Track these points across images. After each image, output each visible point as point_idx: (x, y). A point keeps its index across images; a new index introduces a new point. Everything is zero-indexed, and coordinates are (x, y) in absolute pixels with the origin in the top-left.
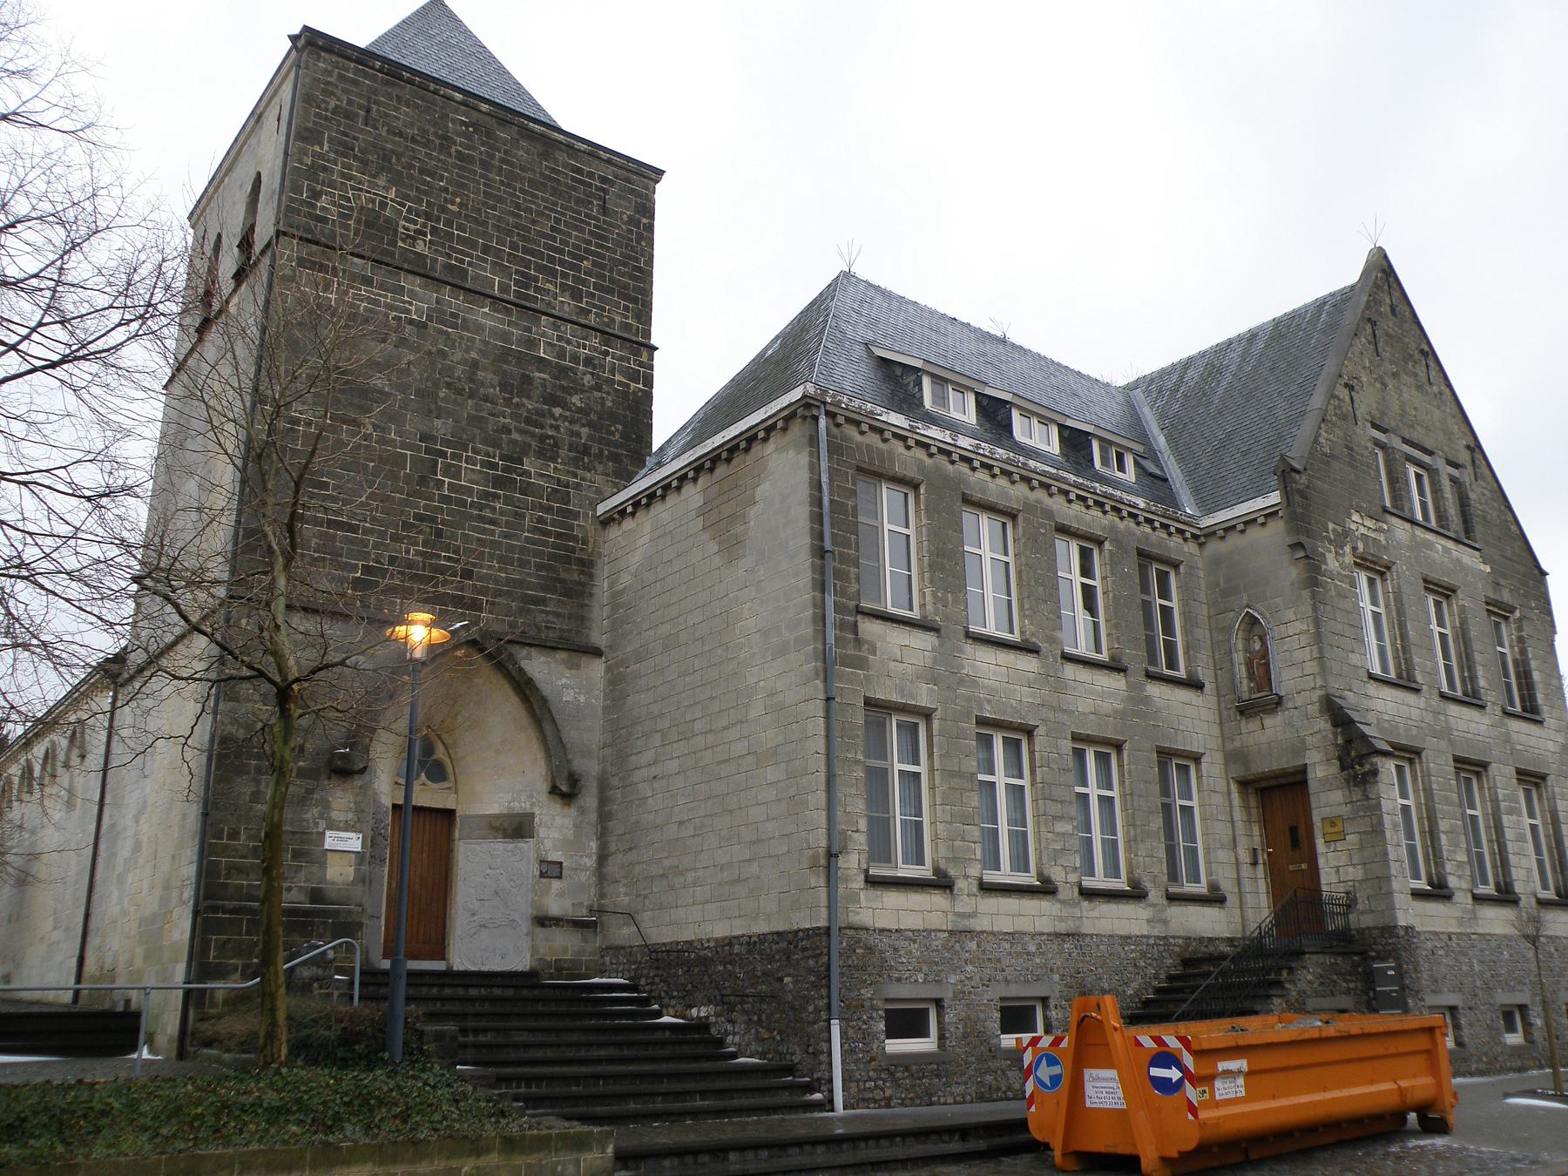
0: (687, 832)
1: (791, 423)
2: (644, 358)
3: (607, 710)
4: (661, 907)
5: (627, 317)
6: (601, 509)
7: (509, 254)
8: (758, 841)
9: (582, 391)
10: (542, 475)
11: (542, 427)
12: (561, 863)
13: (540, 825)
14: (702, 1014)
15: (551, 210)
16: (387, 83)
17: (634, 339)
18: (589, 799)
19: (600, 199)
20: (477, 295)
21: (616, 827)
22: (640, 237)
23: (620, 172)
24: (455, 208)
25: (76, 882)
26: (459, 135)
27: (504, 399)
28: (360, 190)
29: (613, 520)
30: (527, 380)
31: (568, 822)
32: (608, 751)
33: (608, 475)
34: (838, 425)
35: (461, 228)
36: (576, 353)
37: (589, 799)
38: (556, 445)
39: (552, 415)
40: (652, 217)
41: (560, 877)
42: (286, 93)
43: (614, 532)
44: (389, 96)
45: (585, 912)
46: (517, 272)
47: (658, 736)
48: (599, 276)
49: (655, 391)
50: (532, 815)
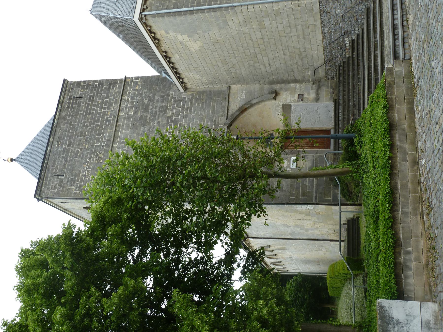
0: (287, 52)
1: (148, 25)
2: (130, 80)
3: (247, 84)
4: (312, 59)
5: (116, 87)
6: (181, 90)
7: (100, 127)
8: (290, 26)
9: (143, 99)
10: (172, 110)
11: (156, 112)
12: (298, 95)
13: (286, 102)
14: (348, 42)
15: (83, 115)
16: (49, 170)
17: (123, 84)
18: (277, 87)
19: (77, 100)
20: (115, 136)
21: (286, 77)
22: (88, 85)
23: (67, 94)
24: (87, 146)
25: (308, 245)
26: (62, 147)
27: (148, 124)
28: (85, 176)
29: (185, 86)
30: (141, 118)
31: (285, 93)
32: (261, 82)
33: (170, 89)
34: (147, 8)
35: (93, 143)
36: (130, 103)
37: (277, 87)
38: (162, 107)
39: (152, 109)
40: (80, 82)
41: (303, 95)
42: (56, 201)
43: (189, 85)
44: (52, 170)
45: (314, 86)
46: (105, 124)
47: (256, 65)
48: (103, 97)
49: (140, 76)
50: (283, 105)
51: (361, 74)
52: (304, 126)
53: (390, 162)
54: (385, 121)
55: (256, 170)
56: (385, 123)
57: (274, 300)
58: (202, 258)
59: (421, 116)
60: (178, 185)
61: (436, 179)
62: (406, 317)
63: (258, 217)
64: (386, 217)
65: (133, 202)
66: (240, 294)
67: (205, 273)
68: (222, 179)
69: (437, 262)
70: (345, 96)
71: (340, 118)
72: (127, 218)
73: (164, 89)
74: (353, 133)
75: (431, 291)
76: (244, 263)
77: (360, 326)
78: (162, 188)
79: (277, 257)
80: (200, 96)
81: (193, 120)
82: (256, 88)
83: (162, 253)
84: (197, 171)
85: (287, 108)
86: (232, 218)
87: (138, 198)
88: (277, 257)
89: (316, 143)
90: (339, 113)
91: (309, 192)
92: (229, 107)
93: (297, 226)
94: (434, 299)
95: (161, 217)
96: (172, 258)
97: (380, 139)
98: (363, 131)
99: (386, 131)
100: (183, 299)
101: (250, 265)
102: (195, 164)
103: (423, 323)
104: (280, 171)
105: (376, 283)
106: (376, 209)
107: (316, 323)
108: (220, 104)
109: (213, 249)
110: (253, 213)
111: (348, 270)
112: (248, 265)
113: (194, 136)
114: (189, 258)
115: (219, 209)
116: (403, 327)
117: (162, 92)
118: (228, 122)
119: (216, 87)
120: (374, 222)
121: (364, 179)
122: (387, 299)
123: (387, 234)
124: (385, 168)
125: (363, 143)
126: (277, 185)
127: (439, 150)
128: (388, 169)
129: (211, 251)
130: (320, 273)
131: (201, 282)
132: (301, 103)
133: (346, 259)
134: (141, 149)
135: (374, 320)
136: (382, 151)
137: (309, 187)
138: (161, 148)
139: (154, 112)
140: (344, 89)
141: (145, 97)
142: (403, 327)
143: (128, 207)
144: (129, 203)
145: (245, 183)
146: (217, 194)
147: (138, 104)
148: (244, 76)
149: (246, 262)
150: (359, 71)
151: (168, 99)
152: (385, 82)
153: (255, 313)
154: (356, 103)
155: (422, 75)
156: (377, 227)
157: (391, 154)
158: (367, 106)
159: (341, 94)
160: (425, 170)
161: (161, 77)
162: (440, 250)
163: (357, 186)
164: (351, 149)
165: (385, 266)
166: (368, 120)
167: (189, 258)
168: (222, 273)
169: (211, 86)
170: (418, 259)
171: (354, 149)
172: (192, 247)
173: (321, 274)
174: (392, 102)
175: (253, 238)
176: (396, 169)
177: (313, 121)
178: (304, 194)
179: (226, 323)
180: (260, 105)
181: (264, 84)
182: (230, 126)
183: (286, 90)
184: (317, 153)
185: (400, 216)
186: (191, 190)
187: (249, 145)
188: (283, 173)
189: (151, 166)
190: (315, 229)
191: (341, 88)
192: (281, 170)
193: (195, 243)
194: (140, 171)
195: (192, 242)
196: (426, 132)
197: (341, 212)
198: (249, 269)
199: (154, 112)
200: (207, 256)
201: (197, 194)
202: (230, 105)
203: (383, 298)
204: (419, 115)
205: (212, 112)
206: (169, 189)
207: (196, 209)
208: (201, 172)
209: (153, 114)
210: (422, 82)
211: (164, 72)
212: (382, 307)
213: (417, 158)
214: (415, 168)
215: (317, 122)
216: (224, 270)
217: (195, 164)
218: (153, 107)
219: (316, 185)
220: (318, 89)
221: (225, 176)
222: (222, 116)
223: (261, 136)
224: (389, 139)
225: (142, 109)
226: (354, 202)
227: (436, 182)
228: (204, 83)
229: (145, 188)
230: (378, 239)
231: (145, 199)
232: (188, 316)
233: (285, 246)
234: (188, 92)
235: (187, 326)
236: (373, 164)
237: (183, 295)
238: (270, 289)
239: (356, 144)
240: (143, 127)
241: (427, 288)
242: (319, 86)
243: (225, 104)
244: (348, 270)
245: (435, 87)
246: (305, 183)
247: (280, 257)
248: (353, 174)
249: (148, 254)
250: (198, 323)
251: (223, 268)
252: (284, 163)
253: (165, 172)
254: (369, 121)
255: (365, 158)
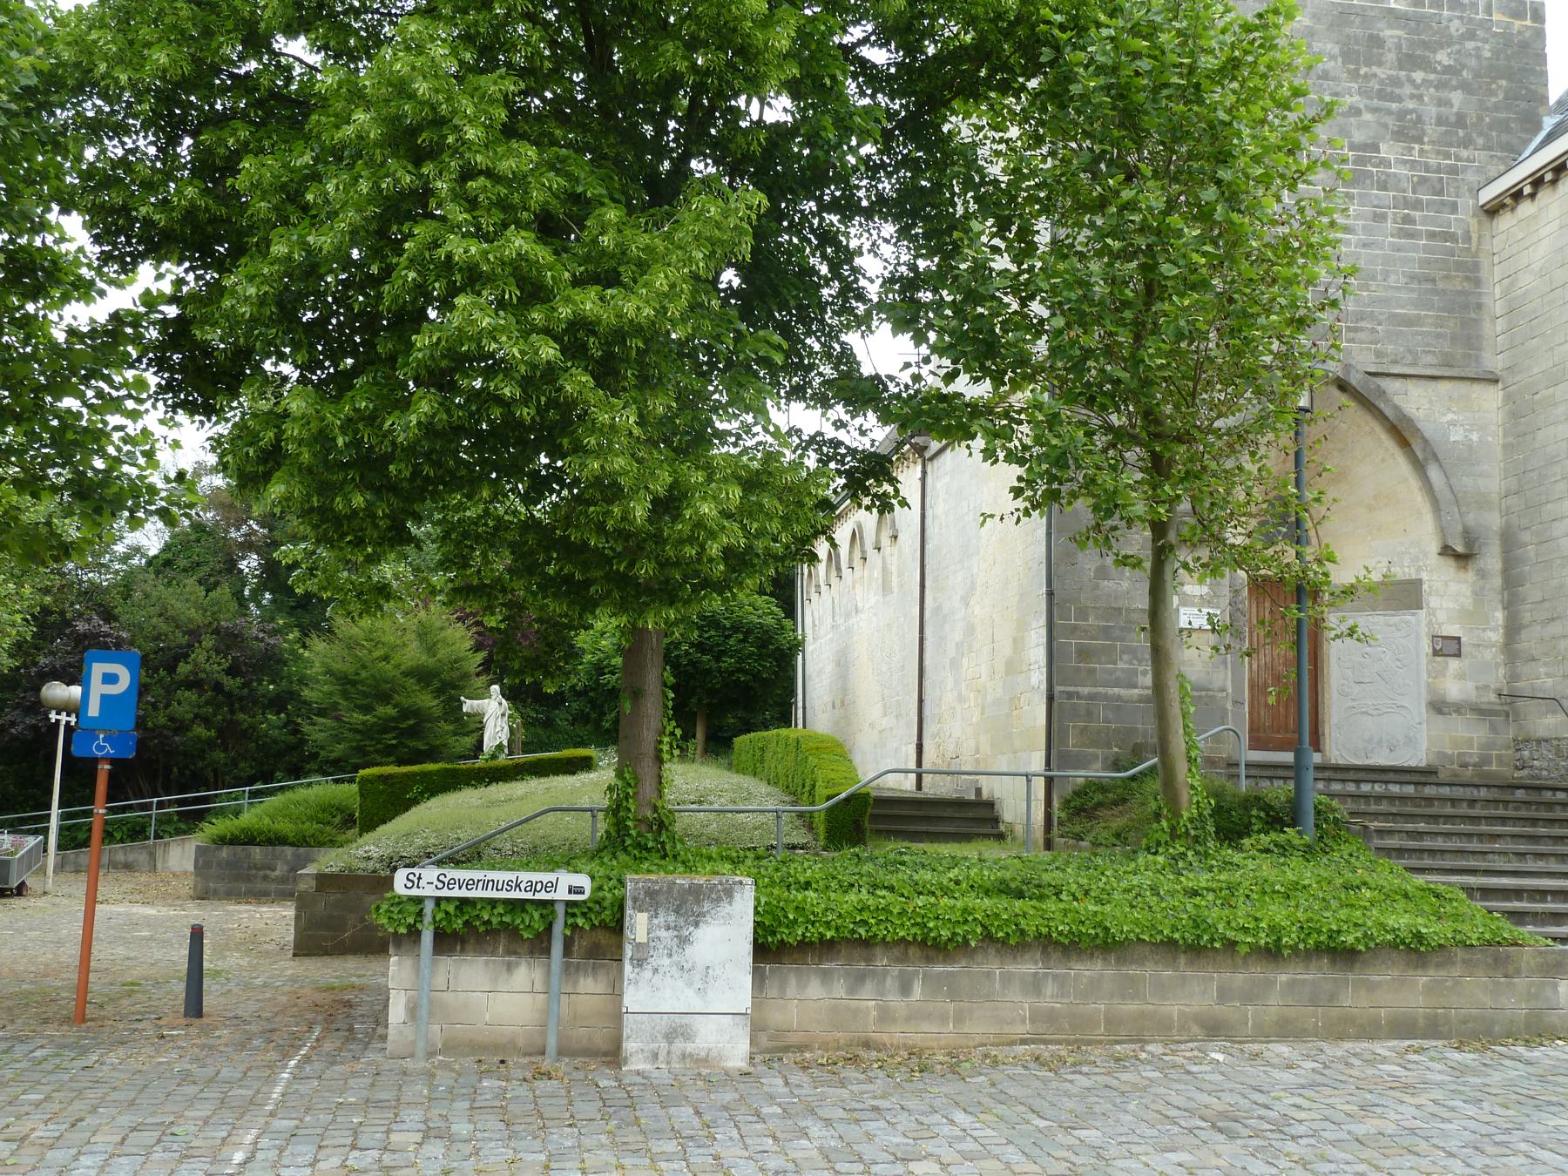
6: (1487, 195)
9: (1449, 46)
10: (1405, 162)
11: (1399, 99)
12: (1458, 639)
18: (1492, 560)
21: (1531, 592)
27: (1349, 72)
29: (1503, 206)
30: (1376, 42)
31: (1466, 589)
32: (1513, 501)
33: (1490, 149)
37: (1492, 560)
38: (1419, 119)
39: (1412, 82)
41: (1458, 655)
43: (1505, 221)
45: (1493, 697)
51: (1540, 865)
52: (1339, 657)
53: (1217, 945)
54: (1365, 935)
55: (1182, 480)
56: (1359, 935)
57: (742, 541)
58: (861, 296)
59: (1384, 1060)
60: (1127, 194)
61: (1161, 1090)
62: (700, 967)
63: (1013, 489)
64: (1023, 922)
65: (1062, 28)
66: (756, 424)
67: (811, 310)
68: (1151, 356)
69: (881, 1074)
70: (1453, 806)
71: (1366, 788)
72: (1002, 10)
73: (1491, 127)
74: (1317, 826)
75: (786, 1049)
76: (848, 443)
77: (662, 825)
78: (1116, 133)
79: (857, 562)
80: (1459, 266)
81: (1365, 245)
82: (1491, 479)
83: (874, 150)
84: (1182, 262)
85: (1406, 595)
86: (1003, 398)
87: (1075, 47)
88: (857, 562)
89: (1278, 695)
90: (1386, 782)
91: (1092, 671)
92: (1414, 381)
93: (970, 630)
94: (758, 1058)
95: (1001, 141)
96: (858, 188)
97: (1299, 914)
98: (1325, 860)
99: (1330, 937)
100: (736, 227)
101: (843, 464)
102: (1204, 254)
103: (686, 1020)
104: (1177, 565)
105: (802, 880)
106: (1046, 892)
107: (665, 685)
108: (1428, 345)
109: (895, 332)
110: (1030, 469)
111: (829, 798)
112: (844, 456)
113: (1310, 246)
114: (860, 247)
115: (1041, 347)
116: (670, 955)
117: (1480, 118)
118: (1355, 380)
119: (1494, 329)
120: (1002, 882)
121: (1150, 857)
122: (756, 913)
123: (966, 921)
124: (1197, 926)
125: (1282, 860)
126: (1126, 557)
127: (1267, 1107)
128: (1190, 938)
129: (887, 327)
130: (804, 708)
131: (785, 291)
132: (1426, 647)
133: (864, 791)
134: (1261, 46)
135: (682, 869)
136: (1256, 919)
137: (1111, 672)
138: (1263, 122)
139: (1397, 91)
140: (1478, 805)
141: (1459, 52)
142: (670, 955)
143: (1042, 11)
144: (1056, 11)
145: (1135, 440)
146: (1093, 339)
147: (1431, 27)
148: (1540, 435)
149: (853, 452)
150: (1552, 859)
151: (1451, 145)
152: (1517, 944)
153: (699, 477)
154: (1427, 843)
155: (1541, 1072)
156: (987, 893)
157: (1244, 949)
158: (1420, 880)
159: (1459, 792)
160: (1189, 1059)
161: (1541, 110)
162: (921, 1086)
163: (1118, 835)
164: (1258, 817)
165: (860, 911)
166: (1369, 880)
167: (860, 247)
168: (812, 367)
169: (1499, 308)
170: (885, 1016)
171: (1255, 828)
172: (898, 258)
173: (800, 712)
174: (1439, 966)
175: (923, 479)
176: (1190, 963)
177: (1357, 689)
178: (1084, 653)
179: (660, 379)
180: (1419, 499)
181: (1507, 512)
182: (1343, 386)
183: (1478, 594)
184: (1235, 702)
185: (1027, 967)
186: (1109, 241)
187: (1273, 453)
188: (1168, 576)
189: (1197, 86)
190: (960, 694)
191: (1483, 793)
192: (1181, 571)
193: (913, 267)
194: (1179, 45)
195: (915, 257)
196: (1326, 1072)
197: (1028, 777)
198: (830, 459)
199: (1397, 91)
200: (868, 313)
201: (1095, 266)
202: (1423, 382)
203: (757, 899)
204: (1387, 1053)
205: (1395, 315)
206: (1110, 163)
207: (1039, 264)
208: (1176, 277)
209: (1389, 89)
210: (1514, 1071)
211: (1558, 125)
212: (729, 893)
213: (1229, 1038)
214: (1195, 1029)
215: (1350, 704)
216: (820, 374)
217: (1204, 254)
218: (1417, 87)
219: (1119, 698)
220: (1480, 711)
221: (1161, 367)
222: (1379, 354)
223: (1309, 495)
224: (1301, 946)
225: (1412, 43)
226: (1061, 823)
227: (1152, 1090)
228: (1512, 283)
229: (1115, 69)
230: (946, 892)
231: (1071, 71)
232: (681, 248)
233: (896, 590)
234: (1479, 223)
235: (647, 247)
236: (1208, 890)
237: (746, 226)
238: (774, 526)
239: (1273, 835)
240: (1336, 50)
241: (794, 1039)
242: (1492, 713)
243: (1425, 366)
244: (829, 798)
245: (1498, 1110)
246: (1125, 657)
247: (858, 573)
248: (1168, 820)
249: (873, 97)
250: (661, 282)
251: (827, 370)
252: (1201, 581)
253: (1176, 140)
254: (1365, 883)
255: (1225, 863)
